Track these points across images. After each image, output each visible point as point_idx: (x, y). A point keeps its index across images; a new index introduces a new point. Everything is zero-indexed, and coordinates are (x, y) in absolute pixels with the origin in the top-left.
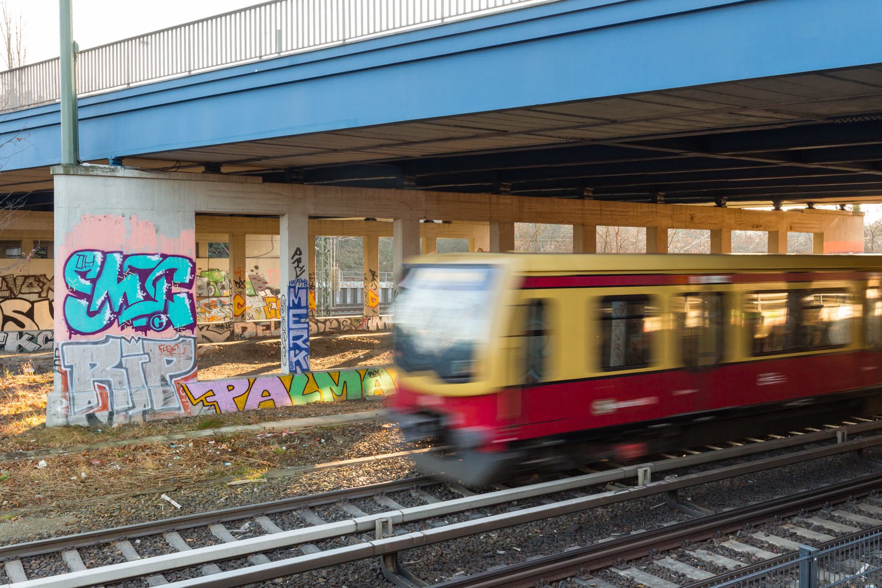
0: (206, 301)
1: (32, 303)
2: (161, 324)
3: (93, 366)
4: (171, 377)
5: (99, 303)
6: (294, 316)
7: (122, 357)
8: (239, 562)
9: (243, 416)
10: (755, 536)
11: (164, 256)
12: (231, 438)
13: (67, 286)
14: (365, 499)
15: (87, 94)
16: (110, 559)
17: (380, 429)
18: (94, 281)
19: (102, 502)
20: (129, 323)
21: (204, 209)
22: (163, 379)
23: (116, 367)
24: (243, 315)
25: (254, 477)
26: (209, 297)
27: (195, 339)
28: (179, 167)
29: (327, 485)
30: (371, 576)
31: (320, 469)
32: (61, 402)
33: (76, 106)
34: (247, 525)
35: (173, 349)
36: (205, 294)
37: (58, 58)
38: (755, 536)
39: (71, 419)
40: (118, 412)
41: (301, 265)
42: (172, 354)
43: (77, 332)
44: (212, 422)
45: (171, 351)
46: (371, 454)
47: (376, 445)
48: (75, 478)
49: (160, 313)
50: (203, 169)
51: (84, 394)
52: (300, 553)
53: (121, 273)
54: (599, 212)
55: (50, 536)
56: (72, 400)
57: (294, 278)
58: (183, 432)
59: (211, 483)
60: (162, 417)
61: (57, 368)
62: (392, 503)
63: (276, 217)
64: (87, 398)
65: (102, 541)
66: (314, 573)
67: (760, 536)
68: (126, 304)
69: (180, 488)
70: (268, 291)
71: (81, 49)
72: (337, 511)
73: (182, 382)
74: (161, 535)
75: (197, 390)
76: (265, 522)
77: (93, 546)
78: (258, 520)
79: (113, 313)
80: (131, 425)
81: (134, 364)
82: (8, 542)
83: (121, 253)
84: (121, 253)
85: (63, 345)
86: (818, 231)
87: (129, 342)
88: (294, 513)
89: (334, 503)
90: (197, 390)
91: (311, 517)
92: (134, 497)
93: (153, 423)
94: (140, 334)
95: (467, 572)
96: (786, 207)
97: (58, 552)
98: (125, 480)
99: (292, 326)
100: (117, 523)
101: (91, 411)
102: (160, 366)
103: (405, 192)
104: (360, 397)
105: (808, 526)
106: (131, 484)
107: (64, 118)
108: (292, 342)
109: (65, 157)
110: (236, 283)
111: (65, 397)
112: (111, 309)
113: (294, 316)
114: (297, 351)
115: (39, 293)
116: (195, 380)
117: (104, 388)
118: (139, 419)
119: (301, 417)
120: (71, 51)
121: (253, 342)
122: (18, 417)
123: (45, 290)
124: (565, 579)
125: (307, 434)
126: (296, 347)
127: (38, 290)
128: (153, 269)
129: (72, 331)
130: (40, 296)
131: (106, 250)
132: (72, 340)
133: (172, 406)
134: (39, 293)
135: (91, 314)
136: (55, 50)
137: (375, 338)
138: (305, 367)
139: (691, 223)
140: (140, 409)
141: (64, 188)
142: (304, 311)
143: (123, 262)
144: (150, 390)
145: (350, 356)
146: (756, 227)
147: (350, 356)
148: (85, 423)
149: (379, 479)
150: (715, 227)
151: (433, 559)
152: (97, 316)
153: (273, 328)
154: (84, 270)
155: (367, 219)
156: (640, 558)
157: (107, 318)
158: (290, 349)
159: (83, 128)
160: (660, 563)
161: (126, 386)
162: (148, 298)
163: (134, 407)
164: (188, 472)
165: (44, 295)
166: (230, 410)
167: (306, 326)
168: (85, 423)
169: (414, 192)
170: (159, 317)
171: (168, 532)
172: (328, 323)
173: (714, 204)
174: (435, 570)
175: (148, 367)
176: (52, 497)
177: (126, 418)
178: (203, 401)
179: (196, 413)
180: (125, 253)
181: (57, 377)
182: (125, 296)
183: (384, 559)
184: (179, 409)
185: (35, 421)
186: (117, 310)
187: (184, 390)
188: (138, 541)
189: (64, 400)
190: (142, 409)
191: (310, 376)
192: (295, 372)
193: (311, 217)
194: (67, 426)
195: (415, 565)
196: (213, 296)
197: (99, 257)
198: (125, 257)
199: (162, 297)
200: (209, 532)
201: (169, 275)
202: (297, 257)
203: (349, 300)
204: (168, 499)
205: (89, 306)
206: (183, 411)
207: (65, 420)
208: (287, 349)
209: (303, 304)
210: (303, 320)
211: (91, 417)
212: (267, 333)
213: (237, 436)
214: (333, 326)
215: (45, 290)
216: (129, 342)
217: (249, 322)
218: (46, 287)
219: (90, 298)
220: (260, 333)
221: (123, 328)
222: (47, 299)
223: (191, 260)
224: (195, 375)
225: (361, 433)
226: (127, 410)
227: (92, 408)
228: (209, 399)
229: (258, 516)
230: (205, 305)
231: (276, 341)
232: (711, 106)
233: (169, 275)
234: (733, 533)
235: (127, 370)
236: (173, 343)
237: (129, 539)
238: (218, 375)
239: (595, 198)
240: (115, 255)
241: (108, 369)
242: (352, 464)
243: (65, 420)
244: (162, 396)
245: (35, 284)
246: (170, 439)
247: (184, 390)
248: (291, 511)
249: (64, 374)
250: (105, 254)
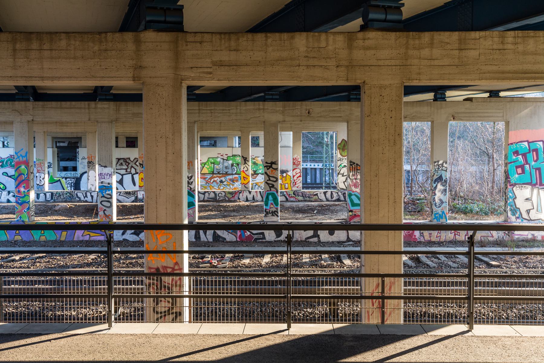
0: (231, 177)
1: (122, 175)
26: (232, 174)
36: (230, 171)
54: (197, 111)
103: (17, 103)
115: (126, 169)
123: (130, 167)
127: (125, 167)
130: (126, 171)
134: (126, 169)
165: (129, 170)
172: (207, 194)
196: (236, 174)
214: (211, 196)
215: (130, 167)
218: (130, 166)
222: (130, 173)
223: (529, 149)
230: (230, 180)
245: (124, 164)
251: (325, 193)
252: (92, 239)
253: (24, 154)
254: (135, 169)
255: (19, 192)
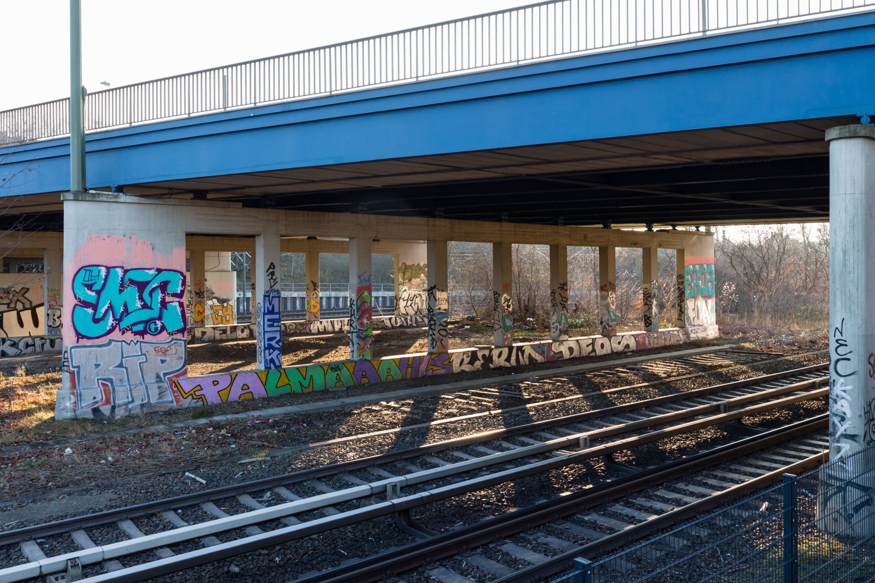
2: (156, 329)
3: (97, 366)
4: (165, 374)
5: (103, 311)
6: (269, 320)
7: (123, 357)
8: (274, 524)
9: (226, 407)
10: (677, 486)
11: (159, 271)
12: (226, 425)
13: (75, 296)
14: (361, 470)
15: (94, 131)
16: (161, 526)
17: (350, 414)
18: (99, 293)
19: (134, 481)
20: (129, 329)
21: (193, 230)
22: (158, 376)
23: (118, 366)
24: (202, 322)
25: (261, 456)
27: (185, 341)
28: (172, 194)
29: (325, 460)
30: (389, 529)
31: (313, 448)
32: (70, 398)
33: (84, 140)
34: (268, 494)
35: (167, 351)
37: (69, 99)
38: (677, 486)
39: (78, 413)
40: (119, 406)
41: (274, 277)
42: (165, 355)
43: (83, 337)
44: (203, 412)
45: (165, 352)
46: (351, 435)
47: (354, 427)
48: (103, 461)
49: (155, 319)
50: (192, 196)
51: (90, 391)
52: (323, 515)
53: (122, 285)
55: (101, 510)
56: (79, 396)
57: (268, 289)
58: (180, 421)
59: (224, 462)
60: (157, 409)
61: (66, 368)
62: (384, 473)
63: (253, 236)
64: (93, 394)
65: (150, 512)
66: (342, 529)
67: (681, 486)
68: (126, 312)
69: (199, 467)
70: (215, 301)
71: (88, 92)
72: (339, 480)
73: (174, 379)
74: (198, 505)
75: (187, 387)
76: (283, 492)
77: (142, 516)
78: (277, 490)
79: (115, 319)
80: (130, 417)
81: (133, 364)
82: (66, 517)
83: (122, 267)
84: (122, 267)
85: (71, 348)
86: (680, 247)
87: (129, 344)
88: (305, 484)
89: (336, 474)
90: (187, 387)
91: (320, 486)
92: (161, 475)
93: (151, 414)
94: (138, 338)
95: (465, 523)
96: (679, 228)
97: (114, 523)
98: (150, 462)
99: (267, 329)
100: (156, 497)
101: (96, 406)
102: (155, 365)
103: (360, 215)
104: (323, 388)
105: (715, 477)
106: (155, 465)
107: (74, 150)
108: (267, 343)
109: (74, 185)
110: (196, 293)
111: (73, 394)
112: (114, 316)
113: (269, 320)
114: (271, 351)
115: (8, 304)
116: (184, 377)
117: (107, 385)
118: (138, 411)
119: (278, 406)
120: (79, 94)
121: (216, 344)
122: (30, 412)
124: (544, 524)
125: (290, 420)
126: (270, 347)
128: (150, 282)
129: (79, 336)
130: (8, 307)
131: (110, 266)
132: (80, 344)
133: (166, 399)
134: (8, 304)
135: (96, 321)
136: (66, 92)
137: (321, 339)
138: (278, 364)
139: (585, 241)
140: (138, 402)
141: (71, 211)
142: (277, 316)
143: (124, 275)
144: (147, 387)
145: (302, 355)
146: (634, 244)
147: (302, 355)
148: (91, 416)
149: (366, 453)
150: (603, 245)
151: (434, 514)
152: (102, 322)
153: (228, 333)
154: (90, 283)
155: (309, 238)
156: (597, 506)
157: (110, 324)
158: (265, 349)
159: (90, 161)
160: (613, 509)
161: (126, 383)
162: (145, 306)
163: (133, 401)
164: (202, 453)
165: (12, 305)
166: (215, 402)
167: (278, 329)
168: (91, 416)
169: (366, 216)
170: (155, 323)
171: (204, 502)
173: (601, 226)
174: (439, 522)
175: (145, 366)
176: (89, 478)
177: (126, 410)
178: (192, 395)
179: (186, 406)
180: (126, 268)
181: (65, 376)
182: (125, 305)
183: (399, 515)
184: (172, 402)
185: (46, 416)
186: (118, 317)
187: (175, 385)
188: (180, 511)
189: (72, 397)
190: (140, 402)
191: (282, 371)
192: (270, 368)
193: (188, 235)
194: (75, 419)
195: (421, 519)
197: (103, 271)
198: (126, 271)
199: (157, 305)
200: (237, 501)
201: (164, 286)
202: (271, 270)
203: (298, 307)
204: (193, 476)
205: (94, 314)
206: (175, 404)
207: (73, 413)
208: (263, 348)
209: (276, 310)
210: (275, 324)
211: (96, 411)
212: (224, 336)
213: (230, 423)
216: (129, 344)
217: (209, 325)
219: (95, 307)
220: (218, 337)
221: (123, 333)
222: (15, 309)
223: (182, 274)
224: (185, 372)
225: (336, 418)
226: (127, 404)
227: (96, 403)
228: (197, 393)
229: (276, 487)
231: (235, 343)
232: (631, 151)
233: (164, 286)
234: (661, 485)
235: (127, 369)
236: (166, 346)
237: (173, 510)
238: (198, 371)
239: (511, 221)
240: (118, 269)
241: (111, 368)
242: (339, 443)
243: (73, 413)
244: (157, 391)
246: (171, 427)
247: (175, 385)
248: (302, 482)
249: (72, 374)
250: (108, 269)
251: (390, 319)
252: (435, 373)
253: (367, 278)
254: (23, 304)
255: (362, 324)
